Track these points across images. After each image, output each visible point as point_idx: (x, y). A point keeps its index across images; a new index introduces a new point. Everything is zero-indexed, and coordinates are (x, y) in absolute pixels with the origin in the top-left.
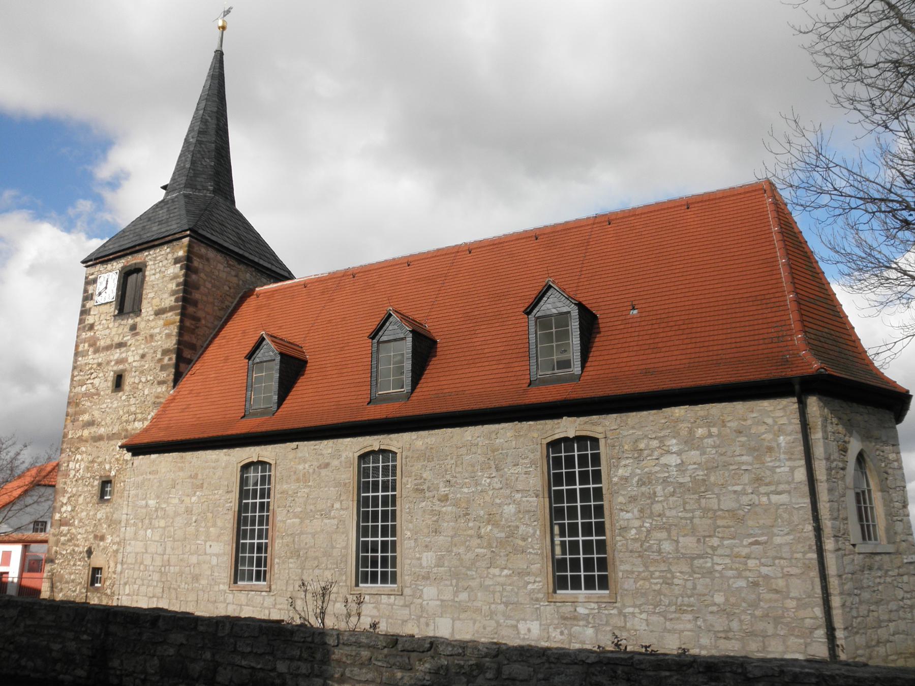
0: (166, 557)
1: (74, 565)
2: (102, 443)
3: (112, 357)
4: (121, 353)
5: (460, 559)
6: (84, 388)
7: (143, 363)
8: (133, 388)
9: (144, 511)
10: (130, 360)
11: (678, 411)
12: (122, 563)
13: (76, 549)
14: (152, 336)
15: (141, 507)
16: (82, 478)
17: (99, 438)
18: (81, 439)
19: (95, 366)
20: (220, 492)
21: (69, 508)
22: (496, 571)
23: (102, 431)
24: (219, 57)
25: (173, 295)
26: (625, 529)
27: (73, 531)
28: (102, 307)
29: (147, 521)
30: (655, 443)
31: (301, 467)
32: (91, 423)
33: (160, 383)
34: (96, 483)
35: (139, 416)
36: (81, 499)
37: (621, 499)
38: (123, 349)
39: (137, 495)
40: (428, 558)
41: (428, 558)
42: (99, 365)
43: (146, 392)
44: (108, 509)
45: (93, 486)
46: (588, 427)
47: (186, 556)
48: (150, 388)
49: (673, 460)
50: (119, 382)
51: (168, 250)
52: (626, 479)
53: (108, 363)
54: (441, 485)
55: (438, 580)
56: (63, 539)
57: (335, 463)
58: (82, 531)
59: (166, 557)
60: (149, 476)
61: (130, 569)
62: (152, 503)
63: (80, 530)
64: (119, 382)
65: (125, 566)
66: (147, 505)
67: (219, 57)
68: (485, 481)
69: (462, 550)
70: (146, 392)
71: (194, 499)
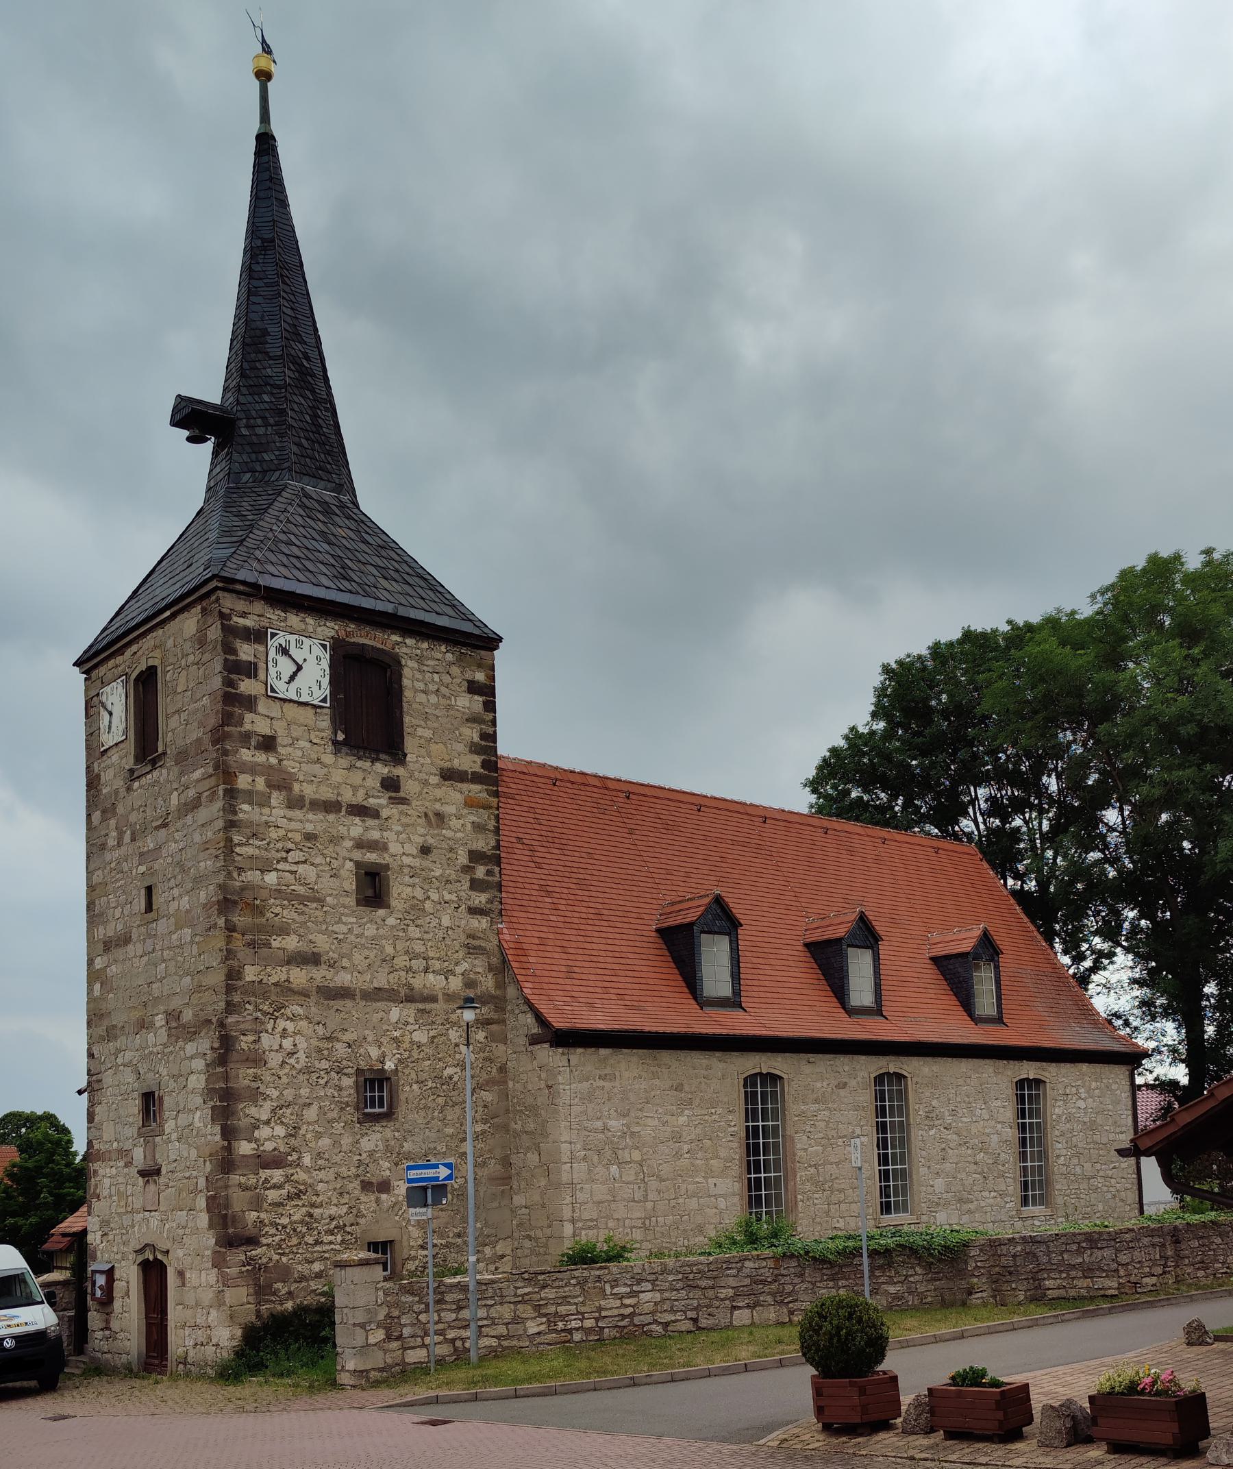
0: (649, 1205)
1: (317, 1243)
2: (349, 1003)
3: (343, 830)
4: (366, 829)
5: (963, 1185)
6: (271, 878)
7: (426, 863)
8: (413, 907)
9: (601, 1136)
10: (394, 848)
11: (1084, 1067)
12: (573, 1221)
13: (317, 1212)
14: (439, 816)
15: (596, 1131)
16: (308, 1070)
17: (344, 993)
18: (285, 988)
19: (298, 837)
20: (719, 1111)
21: (280, 1131)
22: (986, 1194)
23: (344, 979)
24: (265, 144)
25: (477, 753)
26: (1058, 1157)
27: (302, 1176)
28: (301, 710)
29: (608, 1153)
30: (1074, 1090)
31: (819, 1085)
32: (313, 959)
33: (473, 911)
34: (348, 1082)
35: (437, 965)
36: (311, 1114)
37: (1057, 1133)
38: (371, 822)
39: (584, 1112)
40: (939, 1184)
41: (939, 1184)
42: (309, 837)
43: (446, 921)
44: (388, 1133)
45: (340, 1089)
46: (1040, 1072)
47: (681, 1201)
48: (452, 917)
49: (1081, 1104)
50: (373, 887)
51: (449, 656)
52: (1059, 1116)
53: (335, 840)
54: (947, 1113)
55: (947, 1205)
56: (273, 1195)
57: (853, 1083)
58: (328, 1175)
59: (649, 1205)
60: (601, 1083)
61: (590, 1228)
62: (615, 1124)
63: (322, 1175)
64: (373, 887)
65: (579, 1225)
66: (606, 1129)
67: (265, 144)
68: (978, 1112)
69: (963, 1176)
70: (446, 921)
71: (682, 1120)
